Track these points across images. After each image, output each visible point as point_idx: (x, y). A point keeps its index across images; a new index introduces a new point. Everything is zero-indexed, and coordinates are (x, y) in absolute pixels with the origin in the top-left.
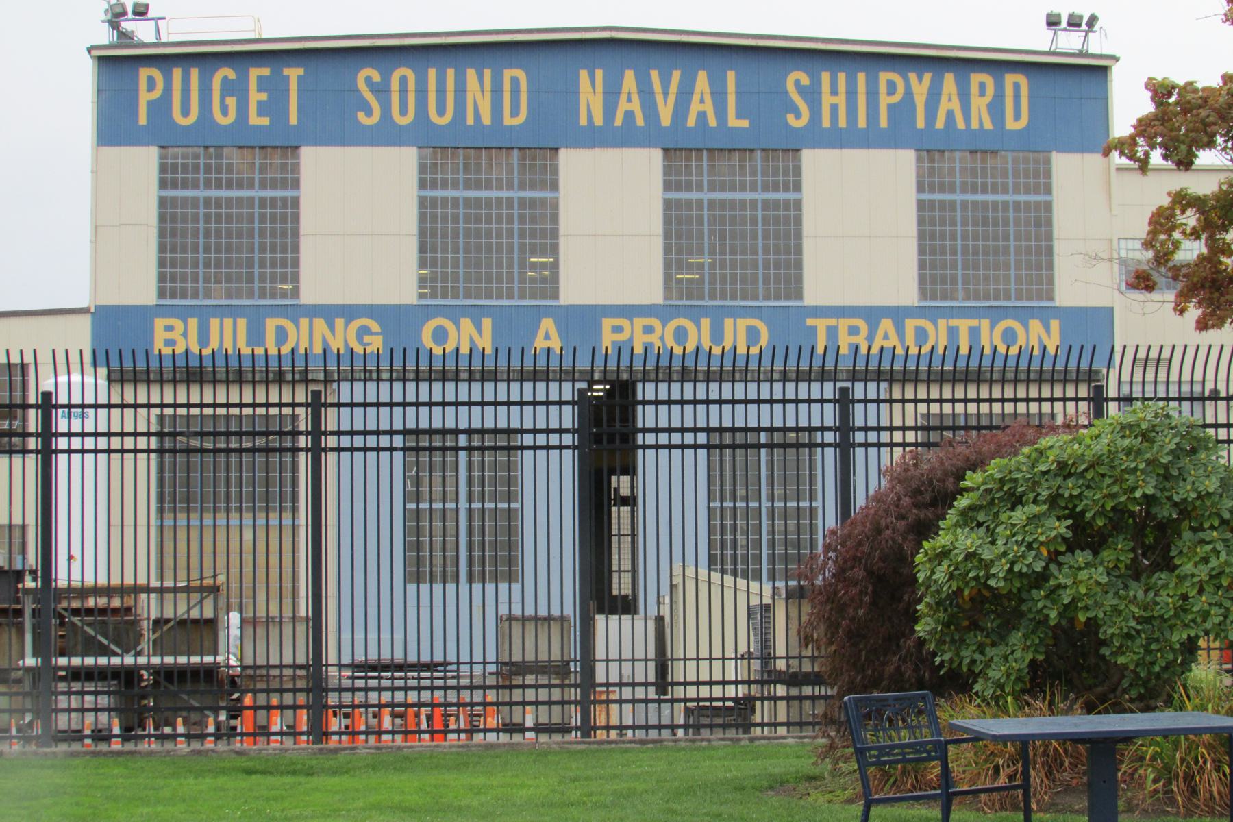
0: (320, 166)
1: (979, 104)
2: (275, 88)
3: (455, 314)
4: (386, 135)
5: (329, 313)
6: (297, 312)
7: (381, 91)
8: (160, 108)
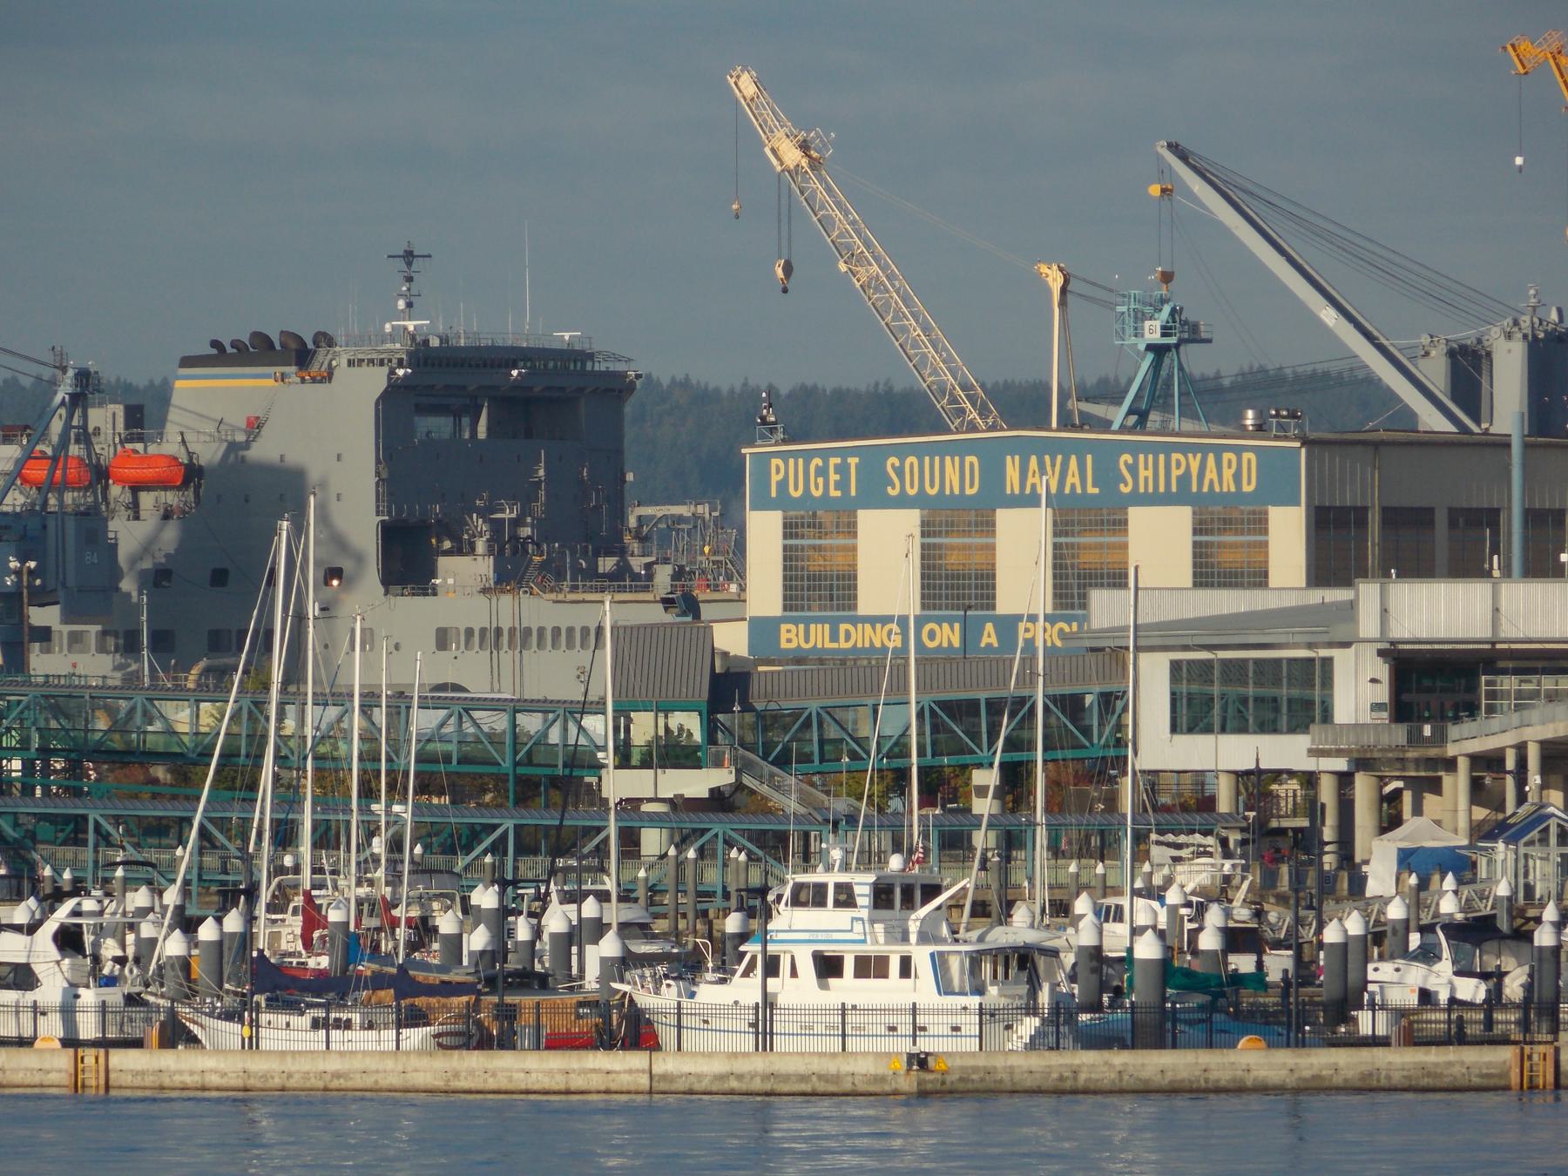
0: (868, 520)
1: (1228, 474)
2: (843, 469)
3: (939, 621)
4: (902, 502)
5: (873, 620)
6: (855, 621)
7: (900, 472)
8: (783, 485)
